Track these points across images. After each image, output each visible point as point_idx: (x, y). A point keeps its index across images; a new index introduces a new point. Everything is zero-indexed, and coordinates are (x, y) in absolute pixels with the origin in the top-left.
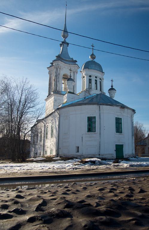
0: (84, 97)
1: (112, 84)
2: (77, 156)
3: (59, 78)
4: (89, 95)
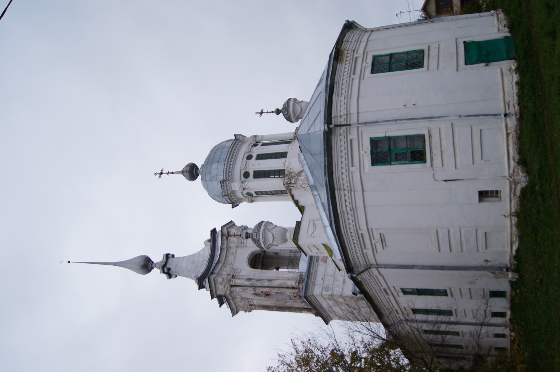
0: (308, 189)
1: (272, 112)
2: (515, 194)
3: (259, 280)
4: (303, 174)
